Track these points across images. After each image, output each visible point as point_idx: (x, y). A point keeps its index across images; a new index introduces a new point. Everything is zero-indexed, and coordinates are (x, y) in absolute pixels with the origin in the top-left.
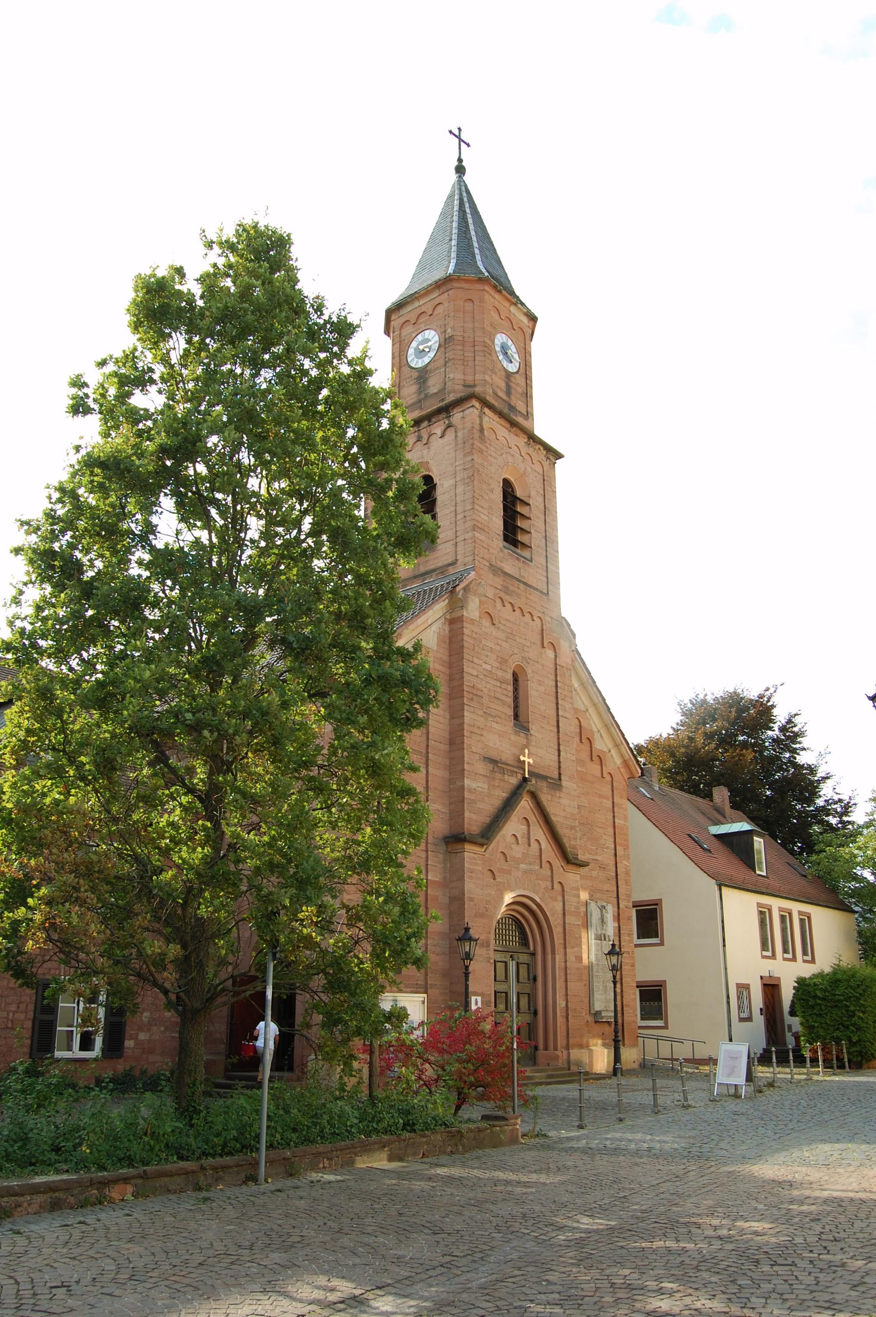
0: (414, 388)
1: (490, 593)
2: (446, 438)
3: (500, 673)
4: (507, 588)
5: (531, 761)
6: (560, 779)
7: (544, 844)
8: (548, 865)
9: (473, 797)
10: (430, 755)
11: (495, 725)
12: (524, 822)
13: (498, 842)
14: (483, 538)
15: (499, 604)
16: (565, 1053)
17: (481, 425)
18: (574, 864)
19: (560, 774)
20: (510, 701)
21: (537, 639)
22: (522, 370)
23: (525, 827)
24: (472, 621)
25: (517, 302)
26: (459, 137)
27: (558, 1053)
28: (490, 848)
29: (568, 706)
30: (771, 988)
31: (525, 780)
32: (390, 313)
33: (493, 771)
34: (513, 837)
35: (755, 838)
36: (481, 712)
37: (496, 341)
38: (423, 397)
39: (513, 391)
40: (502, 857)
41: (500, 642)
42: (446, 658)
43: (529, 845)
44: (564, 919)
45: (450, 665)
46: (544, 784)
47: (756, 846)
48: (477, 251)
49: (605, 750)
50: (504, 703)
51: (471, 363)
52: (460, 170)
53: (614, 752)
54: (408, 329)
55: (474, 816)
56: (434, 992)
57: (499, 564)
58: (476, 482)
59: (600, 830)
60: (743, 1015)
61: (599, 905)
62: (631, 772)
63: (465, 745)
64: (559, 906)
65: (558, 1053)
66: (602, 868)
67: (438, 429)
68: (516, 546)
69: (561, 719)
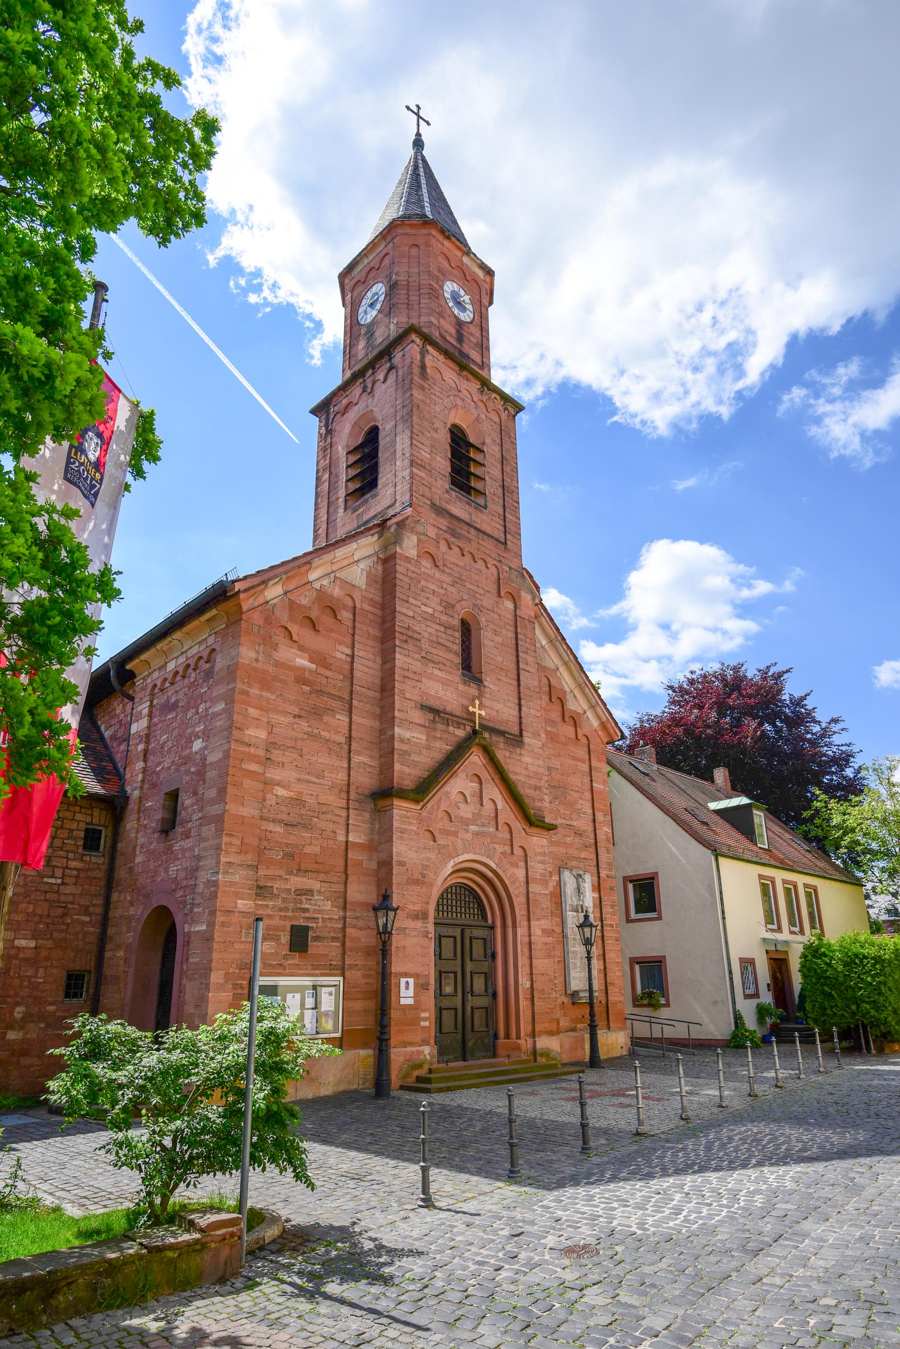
1: (432, 532)
2: (389, 381)
3: (444, 618)
4: (454, 530)
5: (483, 713)
6: (521, 735)
7: (500, 804)
8: (506, 827)
9: (405, 748)
10: (354, 702)
11: (436, 672)
12: (475, 779)
13: (440, 800)
14: (423, 475)
15: (443, 547)
16: (530, 1041)
17: (422, 361)
18: (537, 826)
19: (521, 730)
21: (493, 588)
22: (477, 321)
23: (476, 785)
24: (408, 559)
25: (468, 252)
26: (417, 114)
27: (522, 1042)
28: (429, 806)
29: (530, 659)
30: (779, 964)
31: (475, 732)
32: (342, 277)
33: (434, 721)
34: (460, 796)
35: (755, 812)
36: (417, 656)
37: (445, 288)
39: (465, 340)
40: (446, 817)
41: (445, 586)
42: (378, 599)
43: (482, 805)
44: (528, 888)
45: (383, 607)
46: (501, 739)
47: (756, 820)
49: (580, 711)
50: (449, 650)
51: (416, 307)
52: (418, 143)
53: (589, 714)
54: (360, 288)
55: (407, 770)
56: (355, 975)
57: (444, 505)
58: (414, 418)
59: (575, 795)
60: (747, 992)
61: (575, 873)
62: (610, 735)
63: (396, 691)
64: (520, 873)
65: (522, 1042)
66: (579, 834)
68: (469, 494)
69: (522, 672)
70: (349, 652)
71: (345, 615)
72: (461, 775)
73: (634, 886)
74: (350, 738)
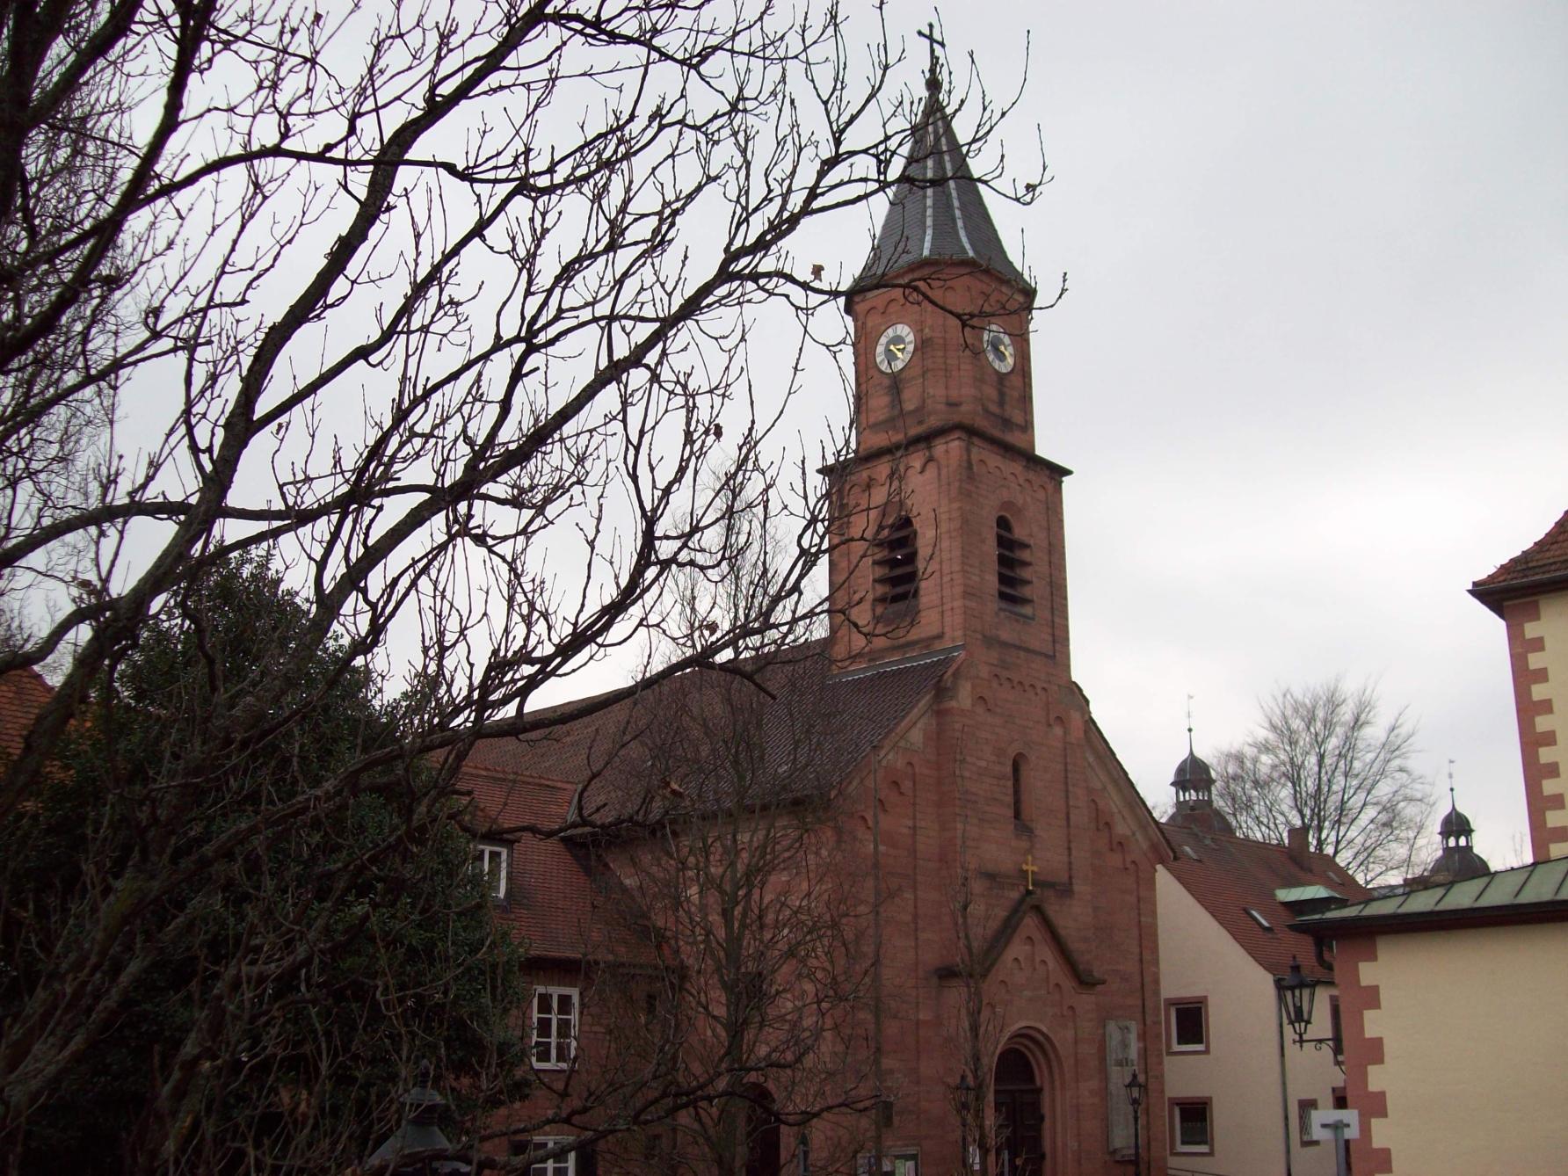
0: (885, 400)
7: (1052, 964)
11: (993, 833)
15: (995, 684)
20: (1010, 799)
31: (1029, 893)
38: (898, 416)
48: (958, 213)
53: (1139, 836)
67: (916, 461)
70: (910, 823)
71: (907, 785)
72: (1016, 940)
73: (1182, 1111)
74: (916, 916)
